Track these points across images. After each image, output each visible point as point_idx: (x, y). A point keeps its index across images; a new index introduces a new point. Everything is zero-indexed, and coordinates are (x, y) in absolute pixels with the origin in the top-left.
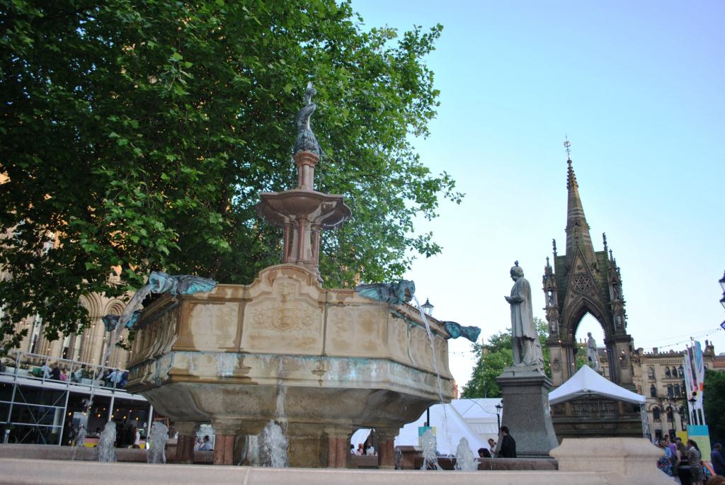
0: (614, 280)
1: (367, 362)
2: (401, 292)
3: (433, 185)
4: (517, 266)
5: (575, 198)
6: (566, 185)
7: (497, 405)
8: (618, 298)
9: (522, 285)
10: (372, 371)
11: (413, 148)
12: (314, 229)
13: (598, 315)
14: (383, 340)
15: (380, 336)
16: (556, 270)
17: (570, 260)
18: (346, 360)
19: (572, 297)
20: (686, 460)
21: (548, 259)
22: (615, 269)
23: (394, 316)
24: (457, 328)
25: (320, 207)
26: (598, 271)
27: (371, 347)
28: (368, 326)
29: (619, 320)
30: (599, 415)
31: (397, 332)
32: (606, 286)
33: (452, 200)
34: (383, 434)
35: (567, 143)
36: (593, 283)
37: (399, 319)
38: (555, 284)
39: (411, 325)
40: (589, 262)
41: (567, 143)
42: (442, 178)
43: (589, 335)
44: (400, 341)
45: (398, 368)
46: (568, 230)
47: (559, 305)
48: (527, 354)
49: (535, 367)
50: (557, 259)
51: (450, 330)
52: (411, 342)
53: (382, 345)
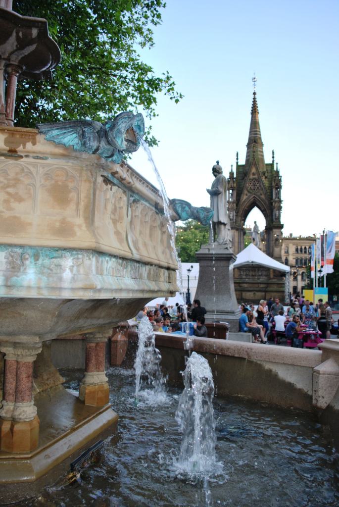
0: (277, 185)
1: (55, 254)
2: (119, 132)
3: (155, 84)
4: (218, 164)
5: (256, 122)
6: (251, 112)
7: (188, 269)
8: (278, 198)
9: (221, 181)
10: (64, 271)
11: (139, 56)
12: (10, 70)
13: (263, 209)
14: (86, 219)
15: (81, 212)
16: (237, 174)
17: (247, 168)
18: (19, 251)
19: (247, 195)
20: (324, 316)
21: (232, 166)
22: (279, 177)
23: (106, 181)
24: (187, 208)
25: (14, 34)
26: (266, 178)
27: (65, 229)
28: (60, 194)
29: (277, 214)
30: (256, 277)
31: (110, 207)
32: (271, 188)
33: (171, 98)
34: (92, 336)
35: (254, 78)
36: (262, 186)
37: (115, 188)
38: (235, 185)
39: (132, 199)
40: (261, 170)
41: (254, 78)
42: (163, 77)
43: (255, 222)
44: (115, 222)
45: (110, 263)
46: (249, 145)
47: (237, 200)
48: (220, 235)
49: (226, 246)
50: (238, 167)
51: (179, 210)
52: (131, 223)
53: (84, 227)
